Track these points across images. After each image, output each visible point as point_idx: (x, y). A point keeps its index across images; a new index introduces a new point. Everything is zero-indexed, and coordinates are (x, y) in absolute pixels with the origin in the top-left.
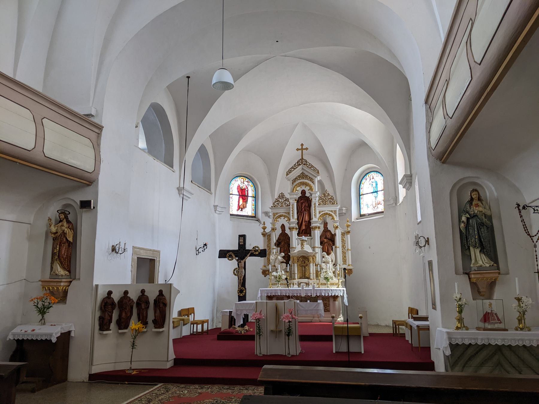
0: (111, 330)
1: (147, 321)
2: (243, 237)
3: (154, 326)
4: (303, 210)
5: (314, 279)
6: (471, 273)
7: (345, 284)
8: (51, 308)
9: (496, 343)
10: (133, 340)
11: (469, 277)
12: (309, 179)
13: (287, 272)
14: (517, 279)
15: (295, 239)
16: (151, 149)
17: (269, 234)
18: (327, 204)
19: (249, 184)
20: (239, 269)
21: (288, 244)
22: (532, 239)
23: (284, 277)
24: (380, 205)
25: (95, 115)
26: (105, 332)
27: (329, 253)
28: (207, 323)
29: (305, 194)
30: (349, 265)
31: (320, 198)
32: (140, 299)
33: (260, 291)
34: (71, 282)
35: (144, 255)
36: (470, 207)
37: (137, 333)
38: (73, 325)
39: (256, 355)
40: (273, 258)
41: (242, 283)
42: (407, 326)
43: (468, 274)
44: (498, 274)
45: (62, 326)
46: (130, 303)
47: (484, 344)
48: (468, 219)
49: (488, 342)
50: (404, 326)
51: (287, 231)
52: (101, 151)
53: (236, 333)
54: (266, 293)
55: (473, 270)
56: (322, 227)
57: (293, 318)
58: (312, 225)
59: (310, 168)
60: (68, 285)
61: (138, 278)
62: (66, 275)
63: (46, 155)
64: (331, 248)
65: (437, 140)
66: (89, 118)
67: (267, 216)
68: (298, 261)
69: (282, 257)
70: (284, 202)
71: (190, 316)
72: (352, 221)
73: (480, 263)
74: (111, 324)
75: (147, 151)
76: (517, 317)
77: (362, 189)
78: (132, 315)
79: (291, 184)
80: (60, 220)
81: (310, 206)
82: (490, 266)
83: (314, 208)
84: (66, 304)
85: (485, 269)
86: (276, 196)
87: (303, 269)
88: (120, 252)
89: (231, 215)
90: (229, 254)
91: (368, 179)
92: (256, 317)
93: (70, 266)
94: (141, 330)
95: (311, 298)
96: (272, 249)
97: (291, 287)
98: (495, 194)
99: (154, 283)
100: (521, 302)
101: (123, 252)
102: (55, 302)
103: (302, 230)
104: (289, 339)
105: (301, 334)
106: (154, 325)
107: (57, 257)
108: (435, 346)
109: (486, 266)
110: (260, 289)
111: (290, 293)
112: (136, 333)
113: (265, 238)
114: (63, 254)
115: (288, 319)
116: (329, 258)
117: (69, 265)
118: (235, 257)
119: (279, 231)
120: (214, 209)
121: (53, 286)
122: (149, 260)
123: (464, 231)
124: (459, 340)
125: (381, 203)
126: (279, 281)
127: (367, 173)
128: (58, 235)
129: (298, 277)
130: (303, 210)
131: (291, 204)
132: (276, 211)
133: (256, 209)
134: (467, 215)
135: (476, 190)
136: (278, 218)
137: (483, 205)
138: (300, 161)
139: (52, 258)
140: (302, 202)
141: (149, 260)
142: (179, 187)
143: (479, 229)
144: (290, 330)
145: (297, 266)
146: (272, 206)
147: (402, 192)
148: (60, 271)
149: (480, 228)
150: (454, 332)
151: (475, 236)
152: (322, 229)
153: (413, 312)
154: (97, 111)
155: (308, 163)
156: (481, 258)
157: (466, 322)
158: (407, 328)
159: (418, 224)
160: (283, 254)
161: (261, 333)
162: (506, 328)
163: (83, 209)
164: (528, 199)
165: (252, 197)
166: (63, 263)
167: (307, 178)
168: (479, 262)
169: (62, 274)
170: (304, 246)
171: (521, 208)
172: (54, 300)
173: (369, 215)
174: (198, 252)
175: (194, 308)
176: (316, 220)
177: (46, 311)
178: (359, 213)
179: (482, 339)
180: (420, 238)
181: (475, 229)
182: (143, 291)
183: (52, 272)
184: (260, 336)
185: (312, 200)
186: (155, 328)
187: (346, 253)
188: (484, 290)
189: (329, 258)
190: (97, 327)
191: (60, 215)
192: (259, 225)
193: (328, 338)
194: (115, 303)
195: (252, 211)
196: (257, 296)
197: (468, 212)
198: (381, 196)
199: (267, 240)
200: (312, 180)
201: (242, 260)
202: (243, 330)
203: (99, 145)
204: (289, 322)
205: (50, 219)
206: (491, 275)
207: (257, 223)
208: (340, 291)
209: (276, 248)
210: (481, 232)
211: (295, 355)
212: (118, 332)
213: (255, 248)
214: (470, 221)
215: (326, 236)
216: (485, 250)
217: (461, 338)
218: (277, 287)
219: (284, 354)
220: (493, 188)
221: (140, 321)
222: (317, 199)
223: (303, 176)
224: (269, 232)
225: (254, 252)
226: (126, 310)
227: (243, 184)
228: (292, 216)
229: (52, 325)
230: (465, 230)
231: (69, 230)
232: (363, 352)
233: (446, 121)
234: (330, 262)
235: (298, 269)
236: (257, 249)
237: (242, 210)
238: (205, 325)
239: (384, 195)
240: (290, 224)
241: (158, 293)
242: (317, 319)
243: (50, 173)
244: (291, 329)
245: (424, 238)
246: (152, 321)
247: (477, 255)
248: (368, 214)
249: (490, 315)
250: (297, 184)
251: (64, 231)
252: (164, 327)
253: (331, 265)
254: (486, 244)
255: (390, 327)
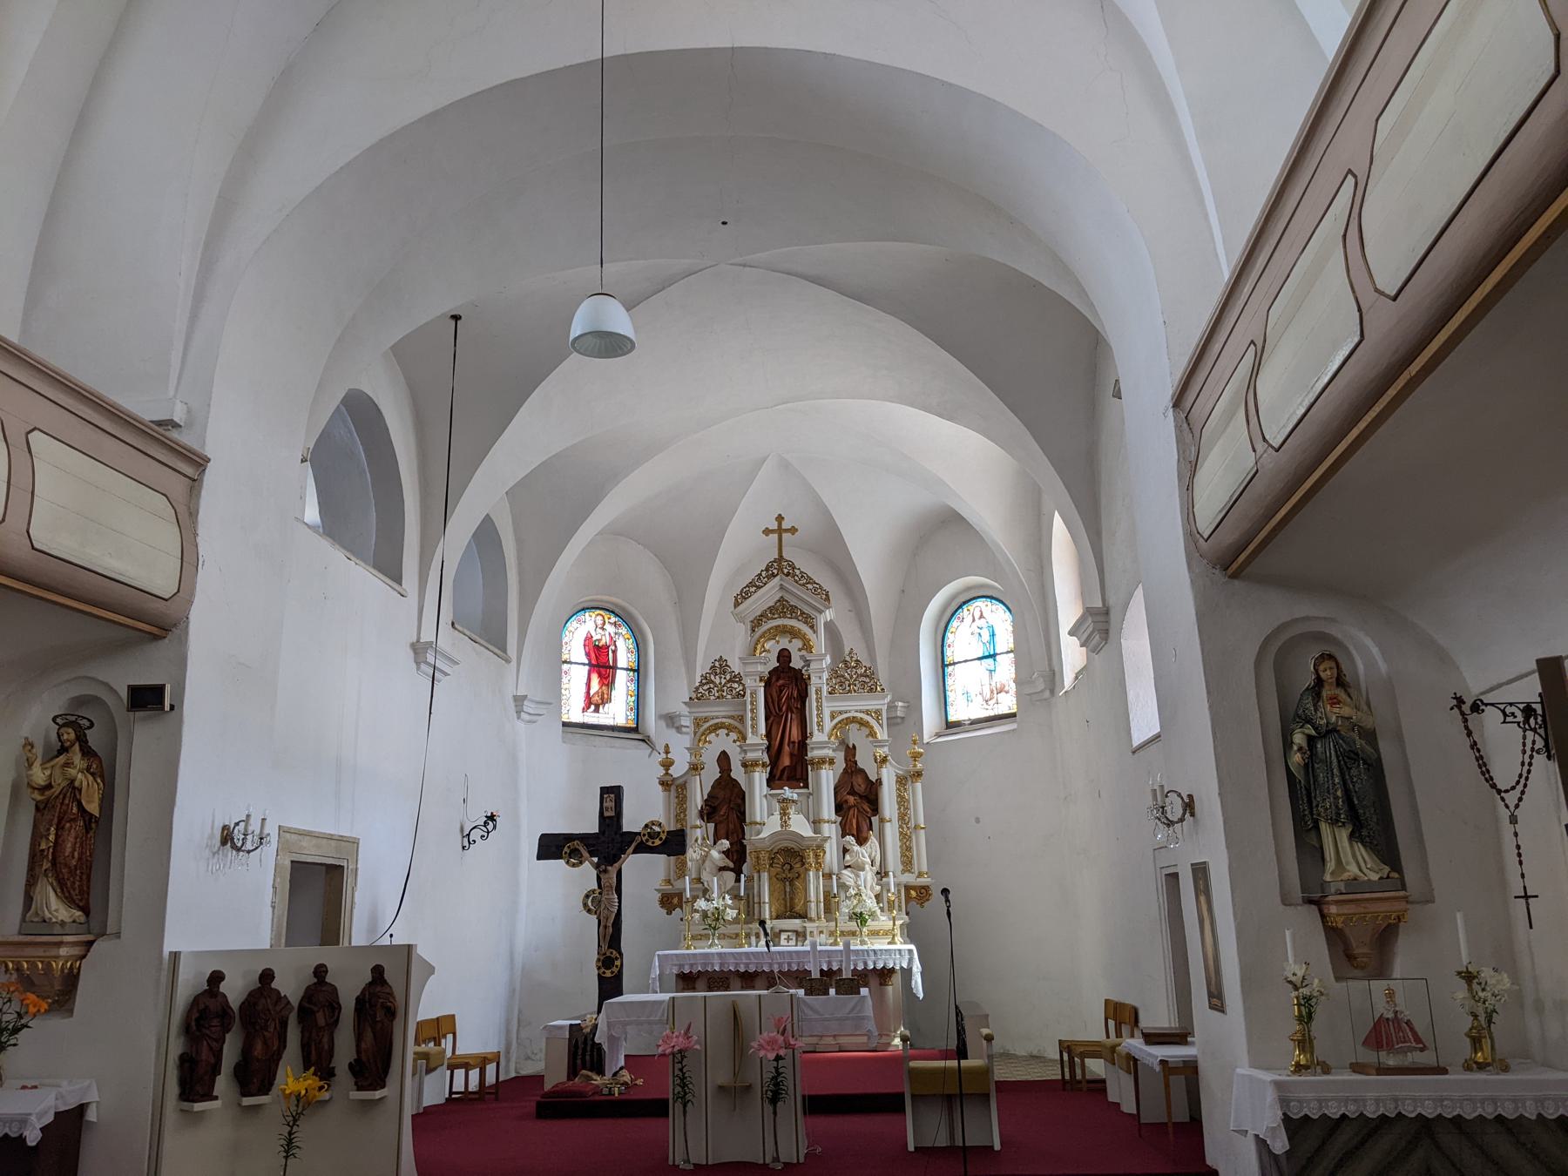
0: (216, 1098)
1: (331, 1066)
2: (612, 795)
3: (356, 1084)
4: (784, 708)
5: (819, 918)
6: (1327, 899)
7: (911, 933)
8: (25, 1029)
9: (1419, 1110)
10: (289, 1128)
11: (1321, 911)
12: (800, 618)
13: (741, 899)
14: (1459, 916)
15: (761, 798)
16: (335, 525)
17: (681, 781)
18: (855, 691)
19: (620, 631)
20: (600, 893)
21: (740, 812)
22: (1503, 799)
23: (731, 914)
24: (1003, 694)
25: (185, 423)
26: (198, 1107)
27: (861, 839)
28: (495, 1064)
29: (790, 661)
30: (920, 875)
31: (835, 673)
32: (309, 995)
33: (656, 958)
34: (90, 943)
35: (312, 853)
36: (1315, 705)
37: (301, 1105)
38: (95, 1088)
39: (674, 1165)
40: (694, 855)
41: (611, 937)
42: (1114, 1059)
43: (1318, 903)
44: (1404, 903)
45: (60, 1089)
46: (278, 1008)
47: (1383, 1114)
48: (1311, 740)
49: (1396, 1108)
50: (1101, 1058)
51: (737, 773)
52: (200, 531)
53: (593, 1094)
54: (676, 965)
55: (1333, 890)
56: (840, 757)
57: (788, 1046)
58: (809, 754)
59: (803, 585)
60: (82, 953)
61: (292, 931)
62: (74, 922)
63: (36, 546)
64: (868, 821)
65: (1220, 511)
66: (167, 434)
67: (673, 726)
68: (771, 865)
69: (724, 852)
70: (729, 685)
71: (443, 1041)
72: (925, 742)
73: (1353, 869)
74: (218, 1078)
75: (321, 530)
76: (1467, 1030)
77: (949, 646)
78: (285, 1047)
79: (749, 633)
80: (62, 746)
81: (803, 695)
82: (1381, 878)
83: (817, 702)
84: (71, 1016)
85: (1369, 886)
86: (702, 667)
87: (788, 890)
88: (249, 846)
89: (565, 724)
90: (569, 847)
91: (968, 619)
92: (673, 1047)
93: (88, 894)
94: (315, 1096)
95: (841, 983)
96: (691, 828)
97: (750, 945)
98: (1383, 666)
99: (338, 944)
100: (1480, 984)
101: (257, 848)
102: (39, 1011)
103: (781, 768)
104: (775, 1113)
105: (813, 1093)
106: (353, 1080)
107: (49, 864)
108: (1232, 1125)
109: (1369, 880)
110: (658, 953)
111: (750, 963)
112: (297, 1106)
113: (670, 795)
114: (67, 854)
115: (773, 1049)
116: (864, 851)
117: (85, 888)
118: (588, 855)
119: (712, 773)
120: (516, 706)
121: (32, 959)
122: (324, 868)
123: (1299, 775)
124: (1312, 1106)
125: (1006, 689)
126: (715, 929)
127: (965, 603)
128: (56, 794)
129: (771, 912)
130: (784, 708)
131: (748, 692)
132: (704, 711)
133: (639, 707)
134: (1309, 728)
135: (1331, 657)
136: (710, 733)
137: (1352, 699)
138: (775, 564)
139: (31, 869)
140: (780, 687)
141: (324, 868)
142: (418, 641)
143: (1345, 769)
144: (777, 1085)
145: (770, 879)
146: (690, 698)
147: (1072, 655)
148: (56, 911)
149: (1347, 767)
150: (1293, 1082)
151: (1336, 791)
152: (841, 765)
153: (1122, 1015)
154: (189, 411)
155: (797, 572)
156: (1354, 856)
157: (1321, 1050)
158: (1114, 1064)
159: (1134, 752)
160: (725, 844)
161: (689, 1097)
162: (1441, 1065)
163: (137, 713)
164: (1474, 686)
165: (627, 669)
166: (66, 884)
167: (794, 614)
168: (1348, 868)
169: (62, 921)
170: (789, 819)
171: (1466, 708)
172: (35, 1006)
173: (973, 722)
174: (467, 840)
175: (453, 1016)
176: (821, 740)
177: (8, 1040)
178: (944, 718)
179: (1377, 1101)
180: (1167, 796)
181: (1332, 771)
182: (320, 971)
183: (31, 912)
184: (685, 1106)
185: (809, 678)
186: (360, 1088)
187: (910, 837)
188: (1365, 950)
189: (864, 851)
190: (173, 1088)
191: (62, 730)
192: (650, 756)
193: (891, 1104)
194: (232, 1009)
195: (628, 714)
196: (650, 975)
197: (1308, 721)
198: (1006, 669)
199: (674, 801)
200: (808, 620)
201: (611, 865)
202: (616, 1084)
203: (193, 514)
204: (778, 1058)
205: (29, 745)
206: (1383, 907)
207: (644, 750)
208: (900, 954)
209: (703, 824)
210: (1351, 778)
211: (795, 1161)
212: (239, 1105)
213: (651, 828)
214: (1316, 748)
215: (852, 787)
216: (1364, 833)
217: (1316, 1099)
218: (710, 946)
219: (761, 1162)
220: (1375, 651)
221: (313, 1069)
222: (825, 676)
223: (782, 607)
224: (681, 776)
225: (647, 840)
226: (266, 1033)
227: (603, 633)
228: (753, 727)
229: (24, 1087)
230: (1302, 772)
231: (91, 778)
232: (997, 1147)
233: (1258, 457)
234: (867, 867)
235: (772, 889)
236: (657, 829)
237: (597, 710)
238: (491, 1069)
239: (1018, 664)
240: (745, 752)
241: (368, 978)
242: (830, 1041)
243: (42, 598)
244: (782, 1081)
245: (1179, 795)
246: (347, 1067)
247: (1342, 847)
248: (970, 719)
249: (1391, 1023)
250: (765, 632)
251: (72, 781)
252: (387, 1084)
253: (868, 875)
254: (1368, 815)
255: (1043, 1060)
